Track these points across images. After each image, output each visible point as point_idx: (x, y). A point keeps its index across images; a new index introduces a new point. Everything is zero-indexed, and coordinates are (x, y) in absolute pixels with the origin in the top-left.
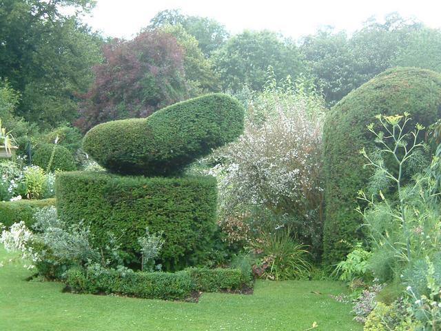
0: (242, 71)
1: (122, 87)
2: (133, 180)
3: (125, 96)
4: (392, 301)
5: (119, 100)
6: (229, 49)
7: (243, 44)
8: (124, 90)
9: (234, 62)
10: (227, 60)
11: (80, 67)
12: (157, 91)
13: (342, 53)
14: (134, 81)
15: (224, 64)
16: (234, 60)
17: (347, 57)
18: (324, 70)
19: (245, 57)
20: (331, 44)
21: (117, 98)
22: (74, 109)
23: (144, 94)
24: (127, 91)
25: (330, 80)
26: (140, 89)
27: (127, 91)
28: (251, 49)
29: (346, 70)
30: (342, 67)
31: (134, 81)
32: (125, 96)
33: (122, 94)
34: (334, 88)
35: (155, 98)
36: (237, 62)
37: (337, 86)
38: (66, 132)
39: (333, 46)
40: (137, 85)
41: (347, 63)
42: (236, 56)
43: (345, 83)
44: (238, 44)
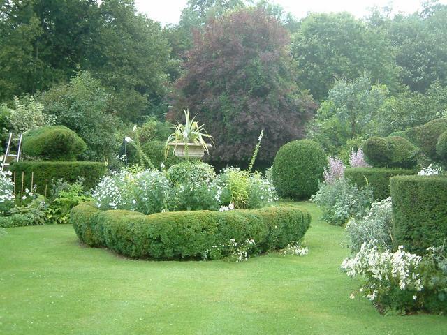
0: (322, 58)
1: (223, 76)
2: (130, 178)
3: (228, 86)
4: (374, 278)
5: (218, 91)
6: (305, 33)
7: (322, 27)
8: (226, 79)
9: (313, 49)
10: (305, 46)
11: (145, 54)
12: (266, 81)
13: (422, 37)
14: (239, 67)
15: (301, 51)
16: (313, 46)
17: (429, 42)
18: (404, 57)
19: (325, 42)
20: (409, 28)
21: (217, 88)
22: (141, 102)
23: (249, 83)
24: (229, 81)
25: (410, 68)
26: (247, 77)
27: (229, 81)
28: (331, 34)
29: (428, 56)
30: (423, 53)
31: (239, 67)
32: (228, 86)
33: (224, 83)
34: (415, 77)
35: (263, 88)
36: (316, 48)
37: (419, 75)
38: (156, 127)
39: (412, 31)
40: (242, 73)
41: (429, 49)
42: (316, 41)
43: (428, 71)
44: (316, 28)
